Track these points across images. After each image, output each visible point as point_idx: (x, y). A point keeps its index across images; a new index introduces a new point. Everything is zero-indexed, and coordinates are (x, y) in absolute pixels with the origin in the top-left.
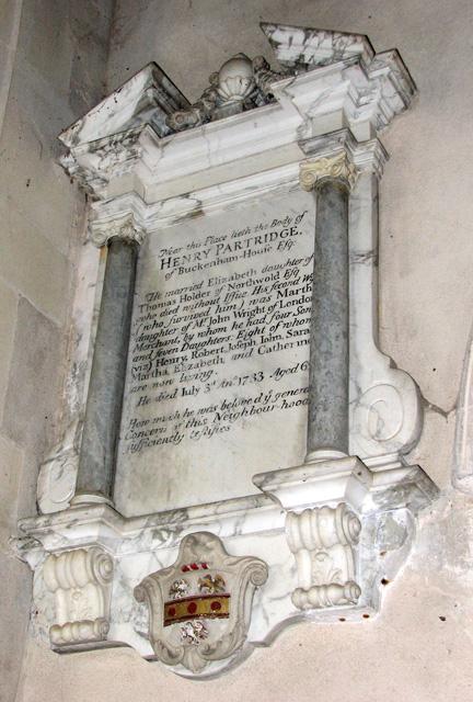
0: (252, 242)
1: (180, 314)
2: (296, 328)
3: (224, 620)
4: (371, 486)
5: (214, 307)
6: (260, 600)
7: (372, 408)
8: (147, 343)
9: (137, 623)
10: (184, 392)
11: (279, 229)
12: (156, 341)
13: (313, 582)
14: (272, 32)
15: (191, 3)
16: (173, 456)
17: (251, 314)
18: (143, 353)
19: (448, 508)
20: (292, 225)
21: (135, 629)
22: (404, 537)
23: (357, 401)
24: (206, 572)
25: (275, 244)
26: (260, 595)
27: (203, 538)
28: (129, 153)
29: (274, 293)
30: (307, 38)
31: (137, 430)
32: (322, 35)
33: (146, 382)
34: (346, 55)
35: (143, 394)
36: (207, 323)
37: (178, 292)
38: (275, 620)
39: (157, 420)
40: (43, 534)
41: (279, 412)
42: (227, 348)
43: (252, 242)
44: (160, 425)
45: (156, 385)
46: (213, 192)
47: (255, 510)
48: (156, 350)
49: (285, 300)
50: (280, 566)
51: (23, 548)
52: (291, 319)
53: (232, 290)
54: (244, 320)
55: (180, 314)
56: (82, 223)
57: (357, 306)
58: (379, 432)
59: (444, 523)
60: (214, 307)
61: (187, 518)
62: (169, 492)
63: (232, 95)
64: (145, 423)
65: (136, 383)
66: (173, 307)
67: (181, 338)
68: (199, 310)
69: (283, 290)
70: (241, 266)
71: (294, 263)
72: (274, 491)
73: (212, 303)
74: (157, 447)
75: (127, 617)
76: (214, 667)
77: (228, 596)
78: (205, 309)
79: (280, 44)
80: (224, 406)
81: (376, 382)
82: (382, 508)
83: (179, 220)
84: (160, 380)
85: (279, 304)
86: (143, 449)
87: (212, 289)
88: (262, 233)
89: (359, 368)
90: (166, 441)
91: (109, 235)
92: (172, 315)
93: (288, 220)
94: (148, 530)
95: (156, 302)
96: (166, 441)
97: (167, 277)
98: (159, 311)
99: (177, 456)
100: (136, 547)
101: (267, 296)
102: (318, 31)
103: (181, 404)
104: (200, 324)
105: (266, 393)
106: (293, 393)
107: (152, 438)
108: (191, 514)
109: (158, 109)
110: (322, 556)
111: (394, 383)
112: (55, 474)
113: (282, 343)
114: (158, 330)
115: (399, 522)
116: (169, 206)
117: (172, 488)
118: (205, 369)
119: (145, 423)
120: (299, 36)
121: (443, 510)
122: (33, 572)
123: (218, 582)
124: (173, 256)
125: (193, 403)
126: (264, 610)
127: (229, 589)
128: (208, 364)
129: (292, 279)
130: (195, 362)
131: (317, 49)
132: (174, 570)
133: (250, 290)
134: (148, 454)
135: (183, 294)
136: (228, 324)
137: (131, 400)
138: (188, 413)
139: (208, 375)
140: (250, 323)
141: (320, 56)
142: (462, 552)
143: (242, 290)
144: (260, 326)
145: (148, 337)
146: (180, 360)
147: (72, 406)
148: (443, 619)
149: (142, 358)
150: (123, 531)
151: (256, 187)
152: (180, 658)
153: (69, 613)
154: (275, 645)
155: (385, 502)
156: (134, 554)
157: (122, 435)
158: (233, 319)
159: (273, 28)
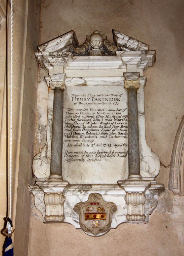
0: (104, 100)
1: (81, 118)
2: (121, 132)
3: (105, 221)
4: (150, 188)
5: (93, 119)
6: (114, 215)
7: (146, 162)
8: (69, 125)
9: (74, 217)
10: (84, 145)
11: (114, 97)
12: (73, 126)
13: (132, 213)
14: (117, 34)
15: (72, 1)
16: (82, 165)
17: (106, 124)
18: (68, 129)
19: (167, 195)
20: (118, 97)
21: (73, 219)
22: (156, 203)
23: (142, 159)
24: (99, 206)
25: (112, 102)
26: (114, 214)
27: (98, 195)
28: (63, 59)
29: (113, 119)
30: (129, 39)
31: (68, 155)
32: (135, 41)
33: (70, 139)
34: (141, 49)
35: (69, 143)
36: (91, 123)
37: (79, 110)
38: (119, 223)
39: (75, 152)
40: (45, 187)
41: (116, 158)
42: (98, 133)
43: (104, 100)
44: (77, 154)
45: (74, 141)
46: (91, 79)
47: (113, 189)
48: (73, 129)
49: (117, 122)
50: (120, 206)
51: (33, 189)
52: (119, 129)
53: (98, 115)
54: (104, 125)
55: (81, 118)
56: (38, 75)
57: (140, 129)
58: (149, 170)
59: (166, 199)
60: (93, 119)
61: (92, 188)
62: (81, 177)
63: (96, 46)
64: (71, 153)
65: (67, 139)
66: (78, 115)
67: (82, 126)
68: (87, 118)
69: (116, 118)
70: (101, 107)
71: (119, 110)
72: (124, 186)
73: (92, 117)
74: (76, 162)
75: (70, 215)
76: (101, 234)
77: (106, 214)
78: (89, 118)
79: (119, 38)
80: (98, 152)
81: (147, 155)
82: (151, 194)
83: (78, 85)
84: (75, 139)
85: (115, 123)
86: (71, 161)
87: (92, 112)
88: (108, 97)
89: (142, 149)
90: (79, 160)
91: (56, 86)
92: (78, 118)
93: (116, 95)
94: (78, 189)
95: (72, 112)
96: (79, 160)
97: (75, 104)
98: (73, 115)
99: (83, 166)
100: (72, 193)
101: (111, 119)
102: (134, 39)
103: (84, 149)
104: (88, 123)
105: (112, 151)
106: (121, 153)
107: (74, 158)
108: (93, 187)
109: (72, 45)
110: (136, 206)
111: (153, 156)
112: (40, 163)
113: (117, 136)
114: (72, 122)
115: (156, 199)
116: (74, 79)
117: (82, 176)
118: (91, 139)
119: (71, 153)
120: (127, 38)
121: (166, 195)
122: (34, 196)
123: (103, 209)
124: (77, 97)
125: (89, 149)
126: (116, 219)
127: (106, 212)
128: (92, 137)
129: (119, 115)
130: (87, 136)
131: (132, 44)
132: (87, 204)
133: (105, 116)
134: (73, 163)
135: (81, 111)
136: (98, 126)
137: (65, 144)
138: (86, 152)
139: (92, 141)
140: (105, 127)
141: (132, 46)
142: (171, 208)
143: (102, 115)
144: (109, 129)
145: (69, 124)
146: (82, 134)
147: (39, 139)
148: (167, 227)
149: (68, 130)
150: (69, 188)
151: (105, 81)
152: (91, 231)
153: (51, 212)
154: (117, 229)
155: (152, 192)
156: (70, 195)
157: (63, 155)
158: (99, 124)
159: (118, 33)
